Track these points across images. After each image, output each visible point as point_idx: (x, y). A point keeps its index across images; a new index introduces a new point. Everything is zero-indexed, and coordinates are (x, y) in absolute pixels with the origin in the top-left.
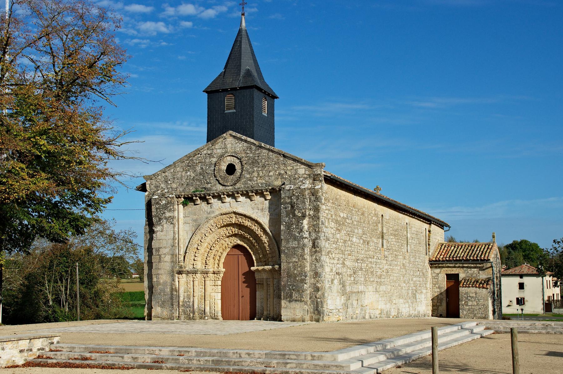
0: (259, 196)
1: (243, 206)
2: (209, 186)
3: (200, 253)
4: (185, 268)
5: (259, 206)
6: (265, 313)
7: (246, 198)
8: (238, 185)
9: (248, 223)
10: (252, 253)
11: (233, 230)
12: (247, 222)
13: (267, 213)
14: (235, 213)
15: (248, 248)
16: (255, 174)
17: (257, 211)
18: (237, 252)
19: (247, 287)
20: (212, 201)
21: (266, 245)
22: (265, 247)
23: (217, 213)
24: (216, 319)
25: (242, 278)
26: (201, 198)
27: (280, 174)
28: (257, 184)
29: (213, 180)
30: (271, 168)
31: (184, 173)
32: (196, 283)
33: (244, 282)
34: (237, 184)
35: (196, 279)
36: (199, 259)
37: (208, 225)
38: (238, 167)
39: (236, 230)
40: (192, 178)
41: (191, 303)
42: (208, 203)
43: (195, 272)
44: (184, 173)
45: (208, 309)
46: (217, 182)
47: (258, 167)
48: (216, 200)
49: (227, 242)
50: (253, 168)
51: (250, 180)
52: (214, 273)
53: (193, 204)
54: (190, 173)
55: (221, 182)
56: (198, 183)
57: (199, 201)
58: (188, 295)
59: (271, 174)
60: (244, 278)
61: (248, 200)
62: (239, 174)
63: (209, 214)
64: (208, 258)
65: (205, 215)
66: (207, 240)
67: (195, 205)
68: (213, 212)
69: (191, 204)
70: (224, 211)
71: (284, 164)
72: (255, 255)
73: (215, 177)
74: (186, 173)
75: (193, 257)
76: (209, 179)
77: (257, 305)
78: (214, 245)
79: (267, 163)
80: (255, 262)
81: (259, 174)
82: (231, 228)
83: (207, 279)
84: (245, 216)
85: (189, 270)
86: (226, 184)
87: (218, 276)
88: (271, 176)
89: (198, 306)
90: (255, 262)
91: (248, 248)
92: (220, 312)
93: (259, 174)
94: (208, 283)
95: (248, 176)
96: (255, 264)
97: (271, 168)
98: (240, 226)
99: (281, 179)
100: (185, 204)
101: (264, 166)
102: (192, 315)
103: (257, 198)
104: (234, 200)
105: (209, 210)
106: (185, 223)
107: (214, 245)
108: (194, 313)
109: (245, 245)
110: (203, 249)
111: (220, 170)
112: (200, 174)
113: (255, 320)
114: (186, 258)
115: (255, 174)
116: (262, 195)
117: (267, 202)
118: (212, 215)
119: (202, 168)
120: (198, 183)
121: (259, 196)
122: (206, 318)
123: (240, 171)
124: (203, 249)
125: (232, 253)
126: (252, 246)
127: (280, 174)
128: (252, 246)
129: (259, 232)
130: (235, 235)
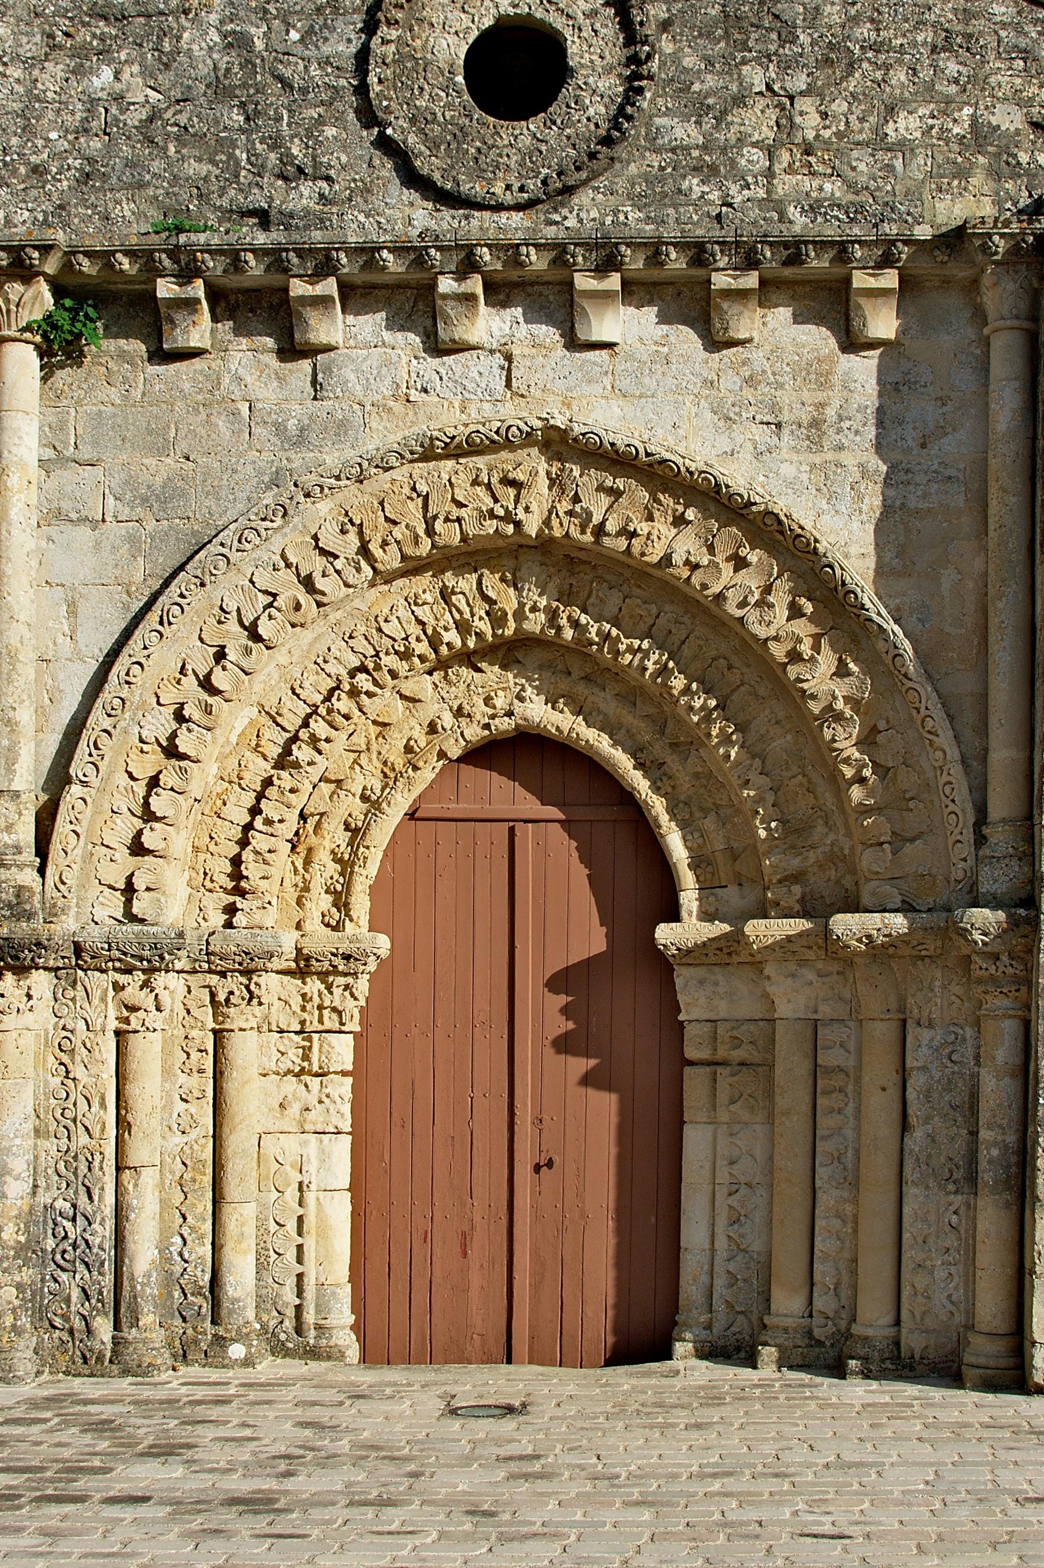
0: (784, 313)
1: (637, 380)
2: (305, 195)
3: (196, 789)
4: (52, 914)
5: (785, 397)
6: (787, 1304)
7: (664, 319)
8: (587, 211)
9: (670, 540)
10: (658, 806)
11: (508, 600)
12: (663, 528)
13: (860, 453)
14: (558, 444)
15: (623, 761)
16: (758, 121)
17: (762, 435)
18: (504, 794)
19: (587, 1080)
20: (329, 328)
21: (845, 740)
22: (826, 758)
23: (382, 435)
24: (313, 1353)
25: (544, 1014)
26: (225, 303)
27: (981, 135)
28: (776, 205)
29: (345, 145)
30: (900, 76)
31: (51, 77)
32: (148, 1051)
33: (563, 1045)
34: (584, 197)
35: (154, 1019)
36: (173, 839)
37: (291, 540)
38: (592, 53)
39: (527, 605)
40: (135, 117)
41: (103, 1233)
42: (292, 349)
43: (150, 961)
44: (51, 77)
45: (241, 1279)
46: (386, 168)
47: (786, 66)
48: (370, 325)
49: (432, 708)
50: (731, 67)
51: (709, 172)
52: (303, 967)
53: (137, 347)
54: (122, 79)
55: (428, 164)
56: (194, 168)
57: (199, 330)
58: (69, 1157)
59: (906, 125)
60: (566, 1011)
61: (686, 339)
62: (598, 109)
63: (300, 440)
64: (259, 841)
65: (263, 455)
66: (257, 685)
67: (161, 355)
68: (342, 427)
69: (115, 353)
70: (450, 420)
71: (1026, 54)
72: (684, 826)
73: (368, 116)
74: (79, 72)
75: (126, 827)
76: (311, 133)
77: (694, 1234)
78: (320, 727)
79: (864, 31)
80: (688, 879)
81: (787, 125)
82: (492, 584)
83: (241, 1017)
84: (658, 475)
85: (93, 937)
86: (475, 189)
87: (338, 997)
88: (904, 147)
89: (163, 1249)
90: (688, 879)
91: (623, 761)
92: (346, 1292)
93: (787, 125)
94: (248, 1051)
95: (686, 132)
96: (689, 899)
97: (900, 76)
98: (569, 565)
99: (995, 175)
100: (59, 348)
101: (836, 58)
102: (104, 1328)
103: (776, 334)
104: (549, 334)
105: (299, 409)
106: (54, 516)
107: (320, 727)
108: (121, 1308)
109: (601, 742)
110: (227, 745)
111: (412, 65)
112: (220, 89)
113: (687, 1368)
114: (62, 827)
115: (758, 121)
116: (832, 306)
117: (863, 370)
118: (332, 459)
119: (238, 42)
120: (194, 168)
121: (784, 313)
122: (237, 1351)
123: (611, 85)
124: (227, 745)
125: (455, 809)
126: (659, 750)
127: (981, 135)
128: (664, 741)
129: (779, 623)
130: (511, 652)
